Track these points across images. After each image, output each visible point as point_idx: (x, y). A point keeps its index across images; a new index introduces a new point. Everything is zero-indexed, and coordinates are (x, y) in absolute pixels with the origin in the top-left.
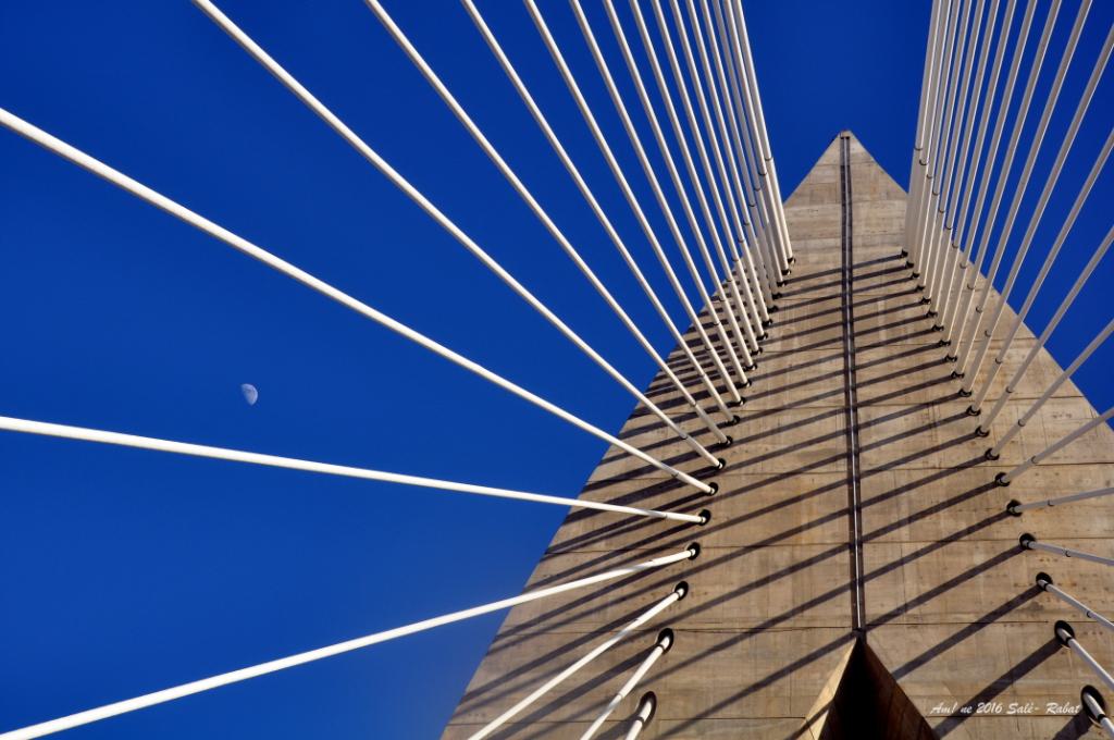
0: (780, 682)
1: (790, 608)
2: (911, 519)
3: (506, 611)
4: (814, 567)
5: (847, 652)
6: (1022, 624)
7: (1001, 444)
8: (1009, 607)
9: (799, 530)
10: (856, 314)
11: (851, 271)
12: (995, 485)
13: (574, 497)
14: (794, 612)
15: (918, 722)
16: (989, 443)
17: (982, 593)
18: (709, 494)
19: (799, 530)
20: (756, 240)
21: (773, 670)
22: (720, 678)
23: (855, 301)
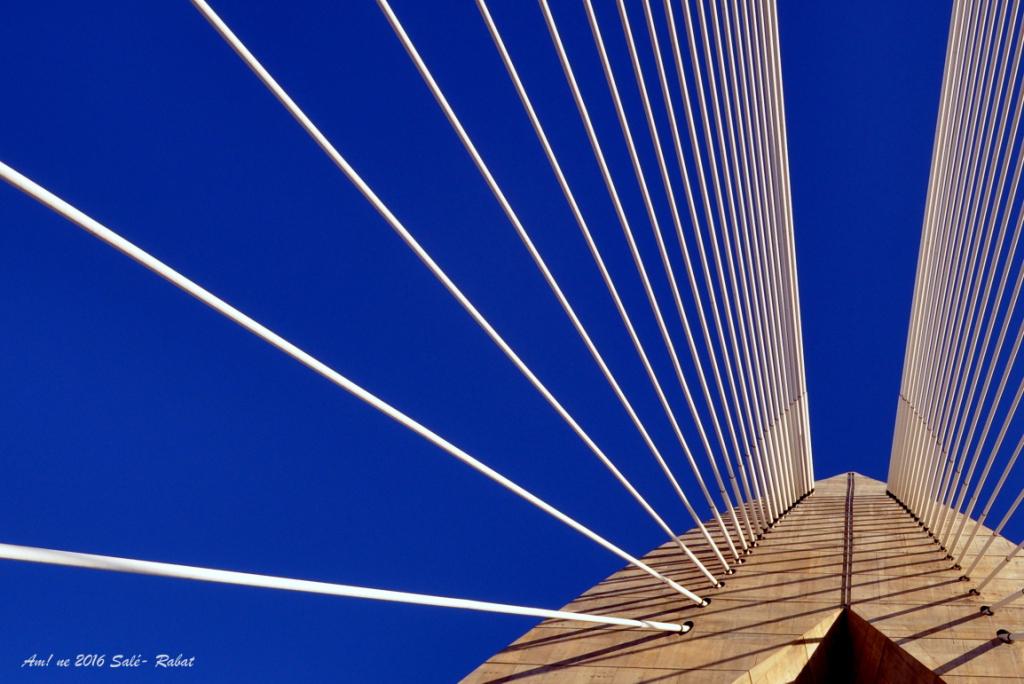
0: (787, 621)
1: (797, 594)
2: (885, 568)
3: (537, 621)
4: (816, 582)
5: (837, 613)
6: (958, 606)
7: (970, 570)
8: (950, 600)
9: (809, 568)
10: (854, 569)
11: (851, 556)
12: (994, 643)
13: (556, 607)
14: (799, 596)
15: (883, 643)
16: (963, 573)
17: (933, 595)
18: (701, 606)
19: (809, 568)
20: (760, 497)
21: (781, 616)
22: (741, 618)
23: (853, 570)
